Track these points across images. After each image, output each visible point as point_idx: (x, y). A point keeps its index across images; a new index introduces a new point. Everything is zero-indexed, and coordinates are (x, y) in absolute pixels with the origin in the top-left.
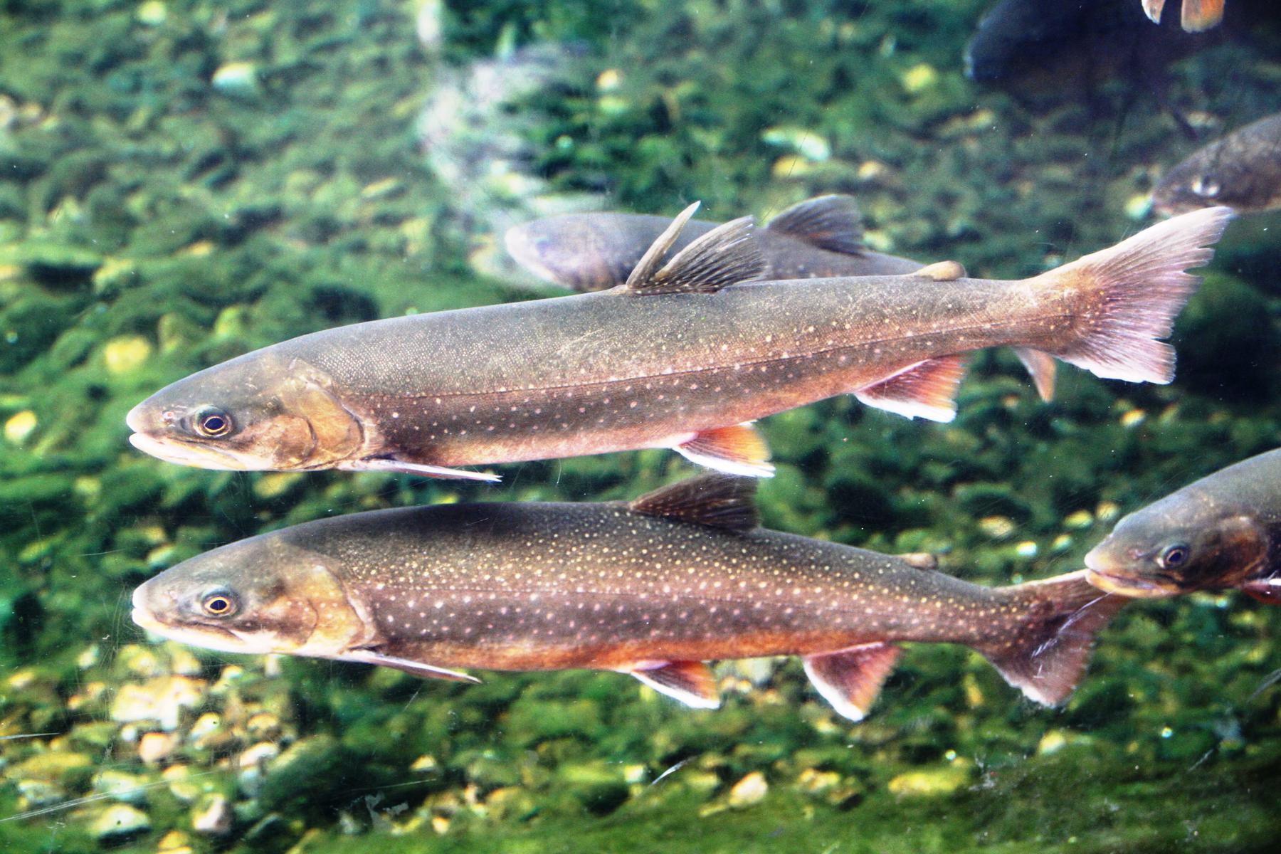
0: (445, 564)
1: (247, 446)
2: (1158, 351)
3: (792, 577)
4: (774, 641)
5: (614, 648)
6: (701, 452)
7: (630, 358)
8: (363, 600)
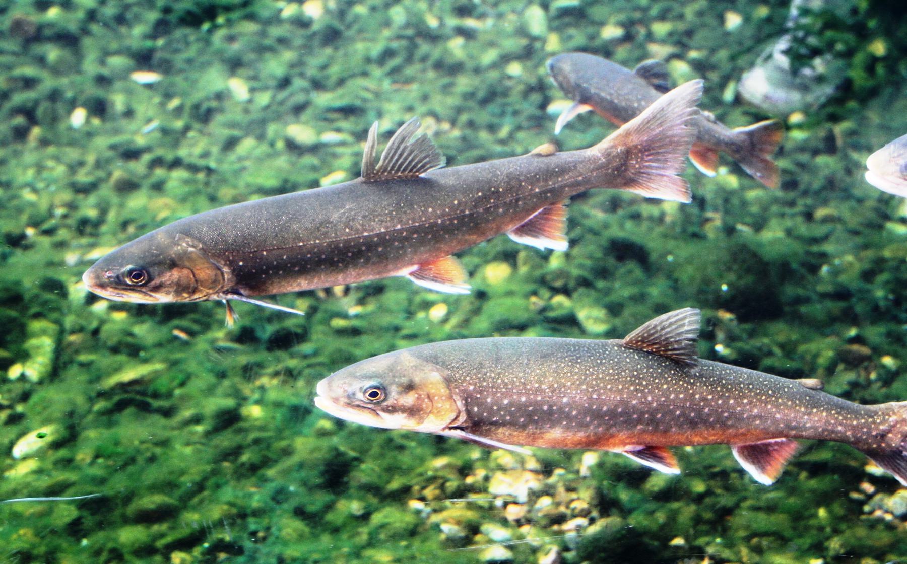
0: (511, 375)
2: (680, 183)
3: (729, 392)
4: (714, 435)
5: (612, 436)
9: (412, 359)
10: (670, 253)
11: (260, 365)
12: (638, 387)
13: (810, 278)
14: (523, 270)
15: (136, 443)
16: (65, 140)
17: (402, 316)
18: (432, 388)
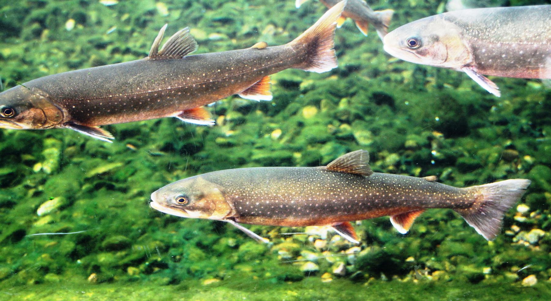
0: (259, 189)
1: (21, 120)
6: (186, 118)
7: (155, 84)
8: (231, 201)
9: (203, 180)
10: (406, 100)
11: (177, 164)
12: (335, 193)
13: (485, 113)
14: (324, 110)
15: (107, 207)
16: (63, 37)
17: (256, 136)
18: (214, 197)
